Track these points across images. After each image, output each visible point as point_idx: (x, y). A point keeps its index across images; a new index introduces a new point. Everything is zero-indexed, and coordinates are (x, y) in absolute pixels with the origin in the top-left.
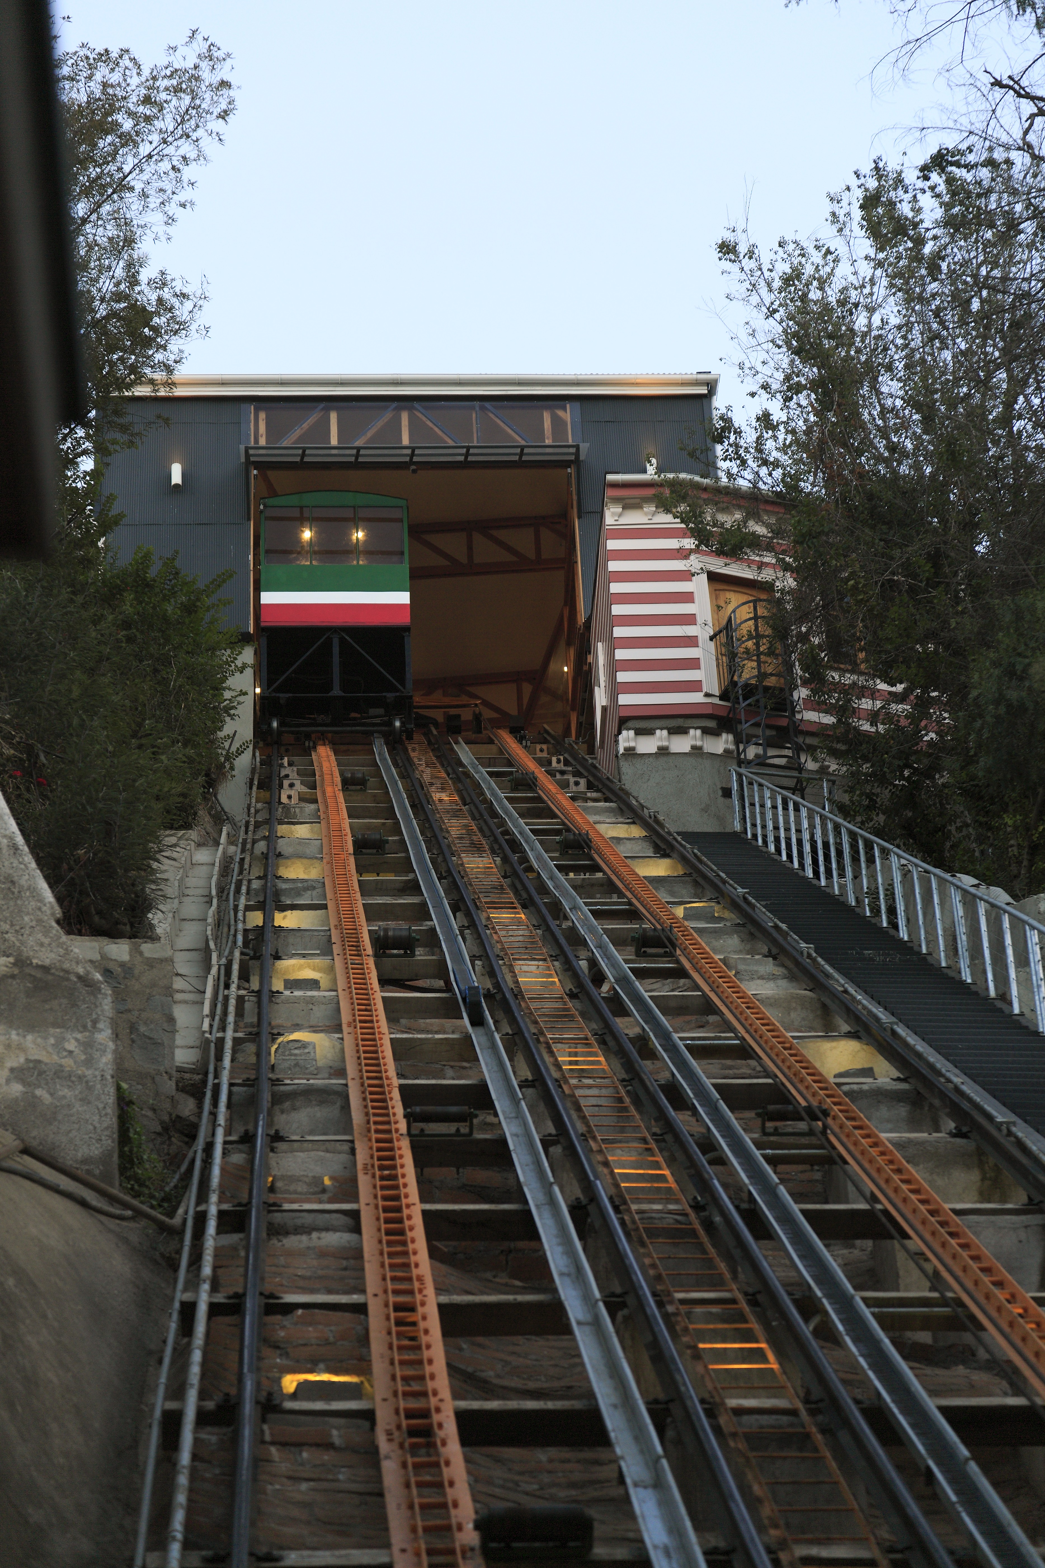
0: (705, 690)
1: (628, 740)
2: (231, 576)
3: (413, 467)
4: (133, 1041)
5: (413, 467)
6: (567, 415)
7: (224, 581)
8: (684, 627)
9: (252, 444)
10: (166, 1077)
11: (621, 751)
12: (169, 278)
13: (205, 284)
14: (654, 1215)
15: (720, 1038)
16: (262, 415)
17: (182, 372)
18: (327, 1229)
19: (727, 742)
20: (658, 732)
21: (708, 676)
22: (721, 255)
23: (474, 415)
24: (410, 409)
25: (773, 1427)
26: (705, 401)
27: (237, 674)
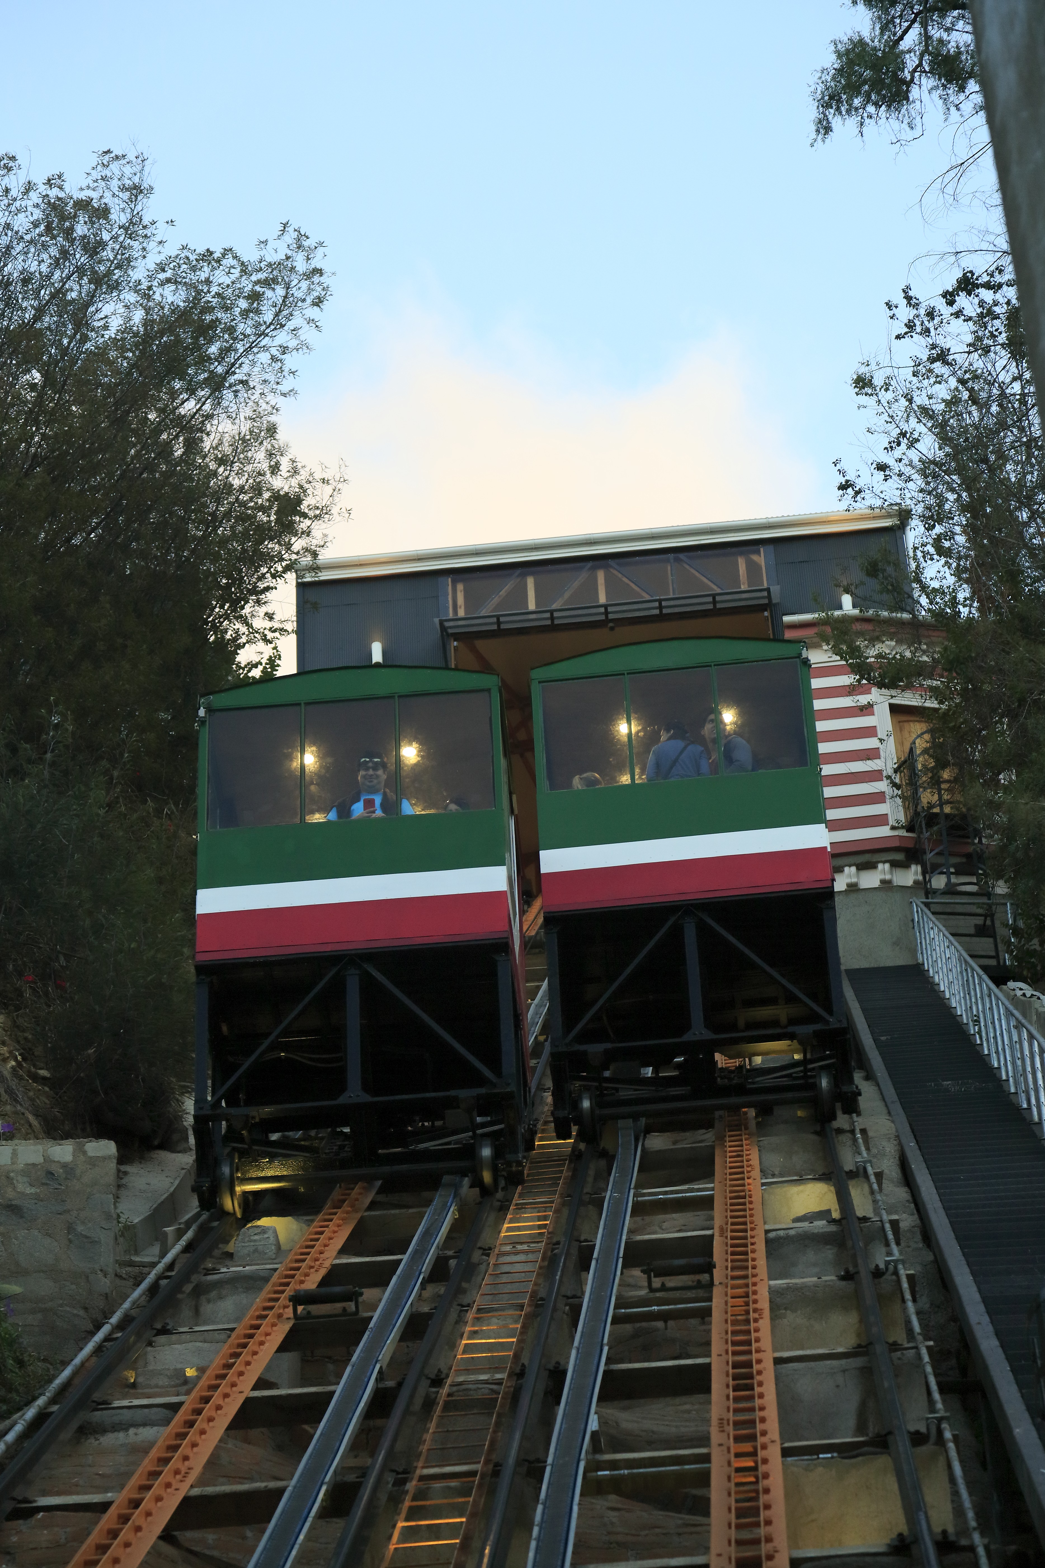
0: (891, 823)
3: (611, 625)
4: (70, 1241)
5: (611, 625)
6: (760, 559)
8: (847, 764)
9: (451, 615)
10: (100, 1275)
12: (299, 465)
13: (343, 467)
14: (470, 1386)
16: (460, 587)
17: (325, 556)
18: (144, 1425)
19: (916, 873)
20: (846, 869)
21: (893, 810)
22: (857, 390)
23: (669, 568)
24: (606, 567)
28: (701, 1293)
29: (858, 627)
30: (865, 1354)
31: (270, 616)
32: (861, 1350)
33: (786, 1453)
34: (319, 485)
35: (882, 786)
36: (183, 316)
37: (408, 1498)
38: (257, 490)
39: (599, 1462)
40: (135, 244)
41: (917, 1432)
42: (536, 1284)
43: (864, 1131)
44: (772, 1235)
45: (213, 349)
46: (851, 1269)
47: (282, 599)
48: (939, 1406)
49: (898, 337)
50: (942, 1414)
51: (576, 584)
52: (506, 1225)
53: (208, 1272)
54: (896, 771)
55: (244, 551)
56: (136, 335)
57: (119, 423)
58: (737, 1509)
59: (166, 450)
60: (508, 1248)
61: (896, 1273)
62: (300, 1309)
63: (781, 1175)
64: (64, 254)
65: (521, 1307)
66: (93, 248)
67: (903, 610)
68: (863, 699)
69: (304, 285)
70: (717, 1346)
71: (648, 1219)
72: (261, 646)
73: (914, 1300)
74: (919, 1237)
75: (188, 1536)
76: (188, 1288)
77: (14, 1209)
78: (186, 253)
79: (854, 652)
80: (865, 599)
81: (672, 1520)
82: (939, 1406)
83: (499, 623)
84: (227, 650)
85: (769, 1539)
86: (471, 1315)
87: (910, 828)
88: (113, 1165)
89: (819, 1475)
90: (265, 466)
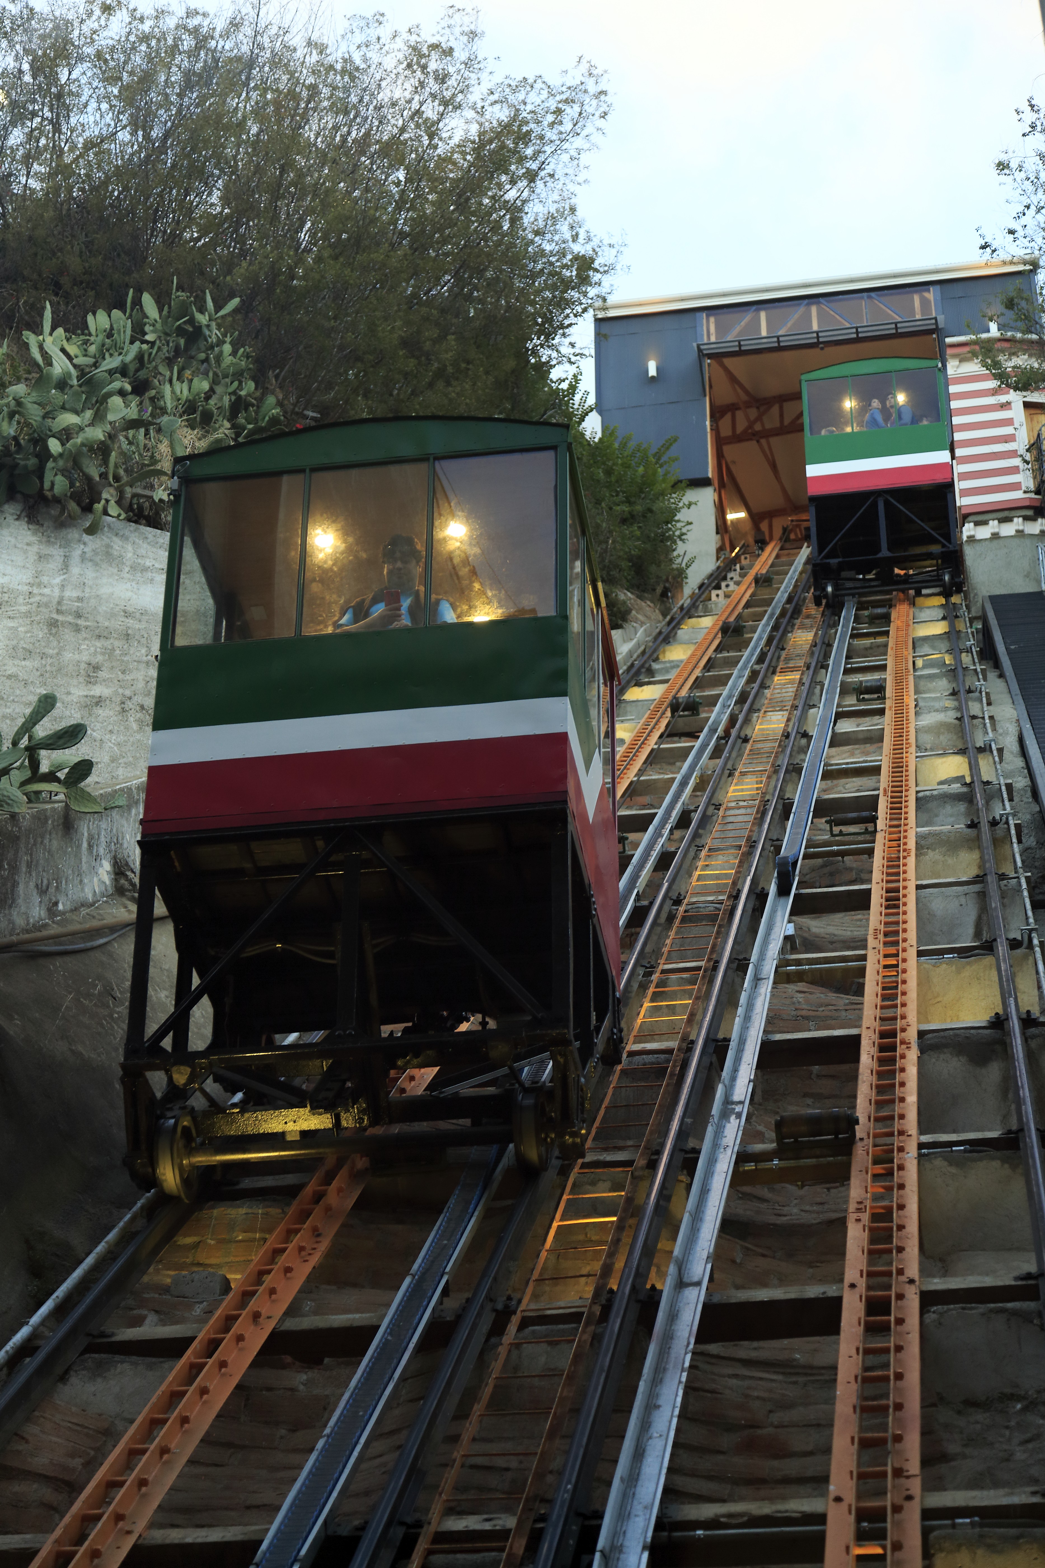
1: (969, 530)
2: (675, 440)
6: (931, 295)
7: (671, 444)
9: (705, 341)
11: (965, 538)
12: (592, 235)
15: (866, 762)
16: (712, 319)
17: (612, 300)
20: (991, 522)
21: (1026, 480)
24: (818, 303)
25: (653, 1063)
26: (1031, 275)
27: (686, 509)
28: (868, 837)
29: (999, 345)
30: (982, 882)
31: (572, 345)
32: (979, 879)
33: (920, 954)
34: (606, 249)
35: (1017, 462)
36: (506, 128)
37: (653, 985)
38: (563, 254)
39: (788, 960)
40: (472, 75)
41: (1015, 939)
42: (751, 831)
43: (991, 718)
44: (921, 795)
45: (529, 152)
46: (976, 821)
47: (582, 332)
48: (1031, 920)
49: (1024, 135)
50: (1033, 926)
51: (796, 316)
52: (732, 788)
54: (1028, 450)
55: (554, 297)
56: (473, 142)
57: (462, 206)
58: (882, 995)
59: (498, 225)
60: (733, 804)
61: (1007, 823)
63: (932, 750)
64: (422, 84)
65: (740, 847)
66: (442, 78)
67: (1032, 332)
68: (1003, 399)
69: (594, 102)
70: (877, 876)
71: (835, 782)
72: (567, 366)
73: (1020, 841)
74: (1029, 794)
78: (507, 82)
79: (996, 364)
80: (1004, 326)
81: (843, 1000)
82: (1031, 920)
83: (740, 346)
84: (544, 369)
85: (903, 1017)
86: (703, 854)
87: (1037, 492)
89: (943, 970)
90: (568, 235)
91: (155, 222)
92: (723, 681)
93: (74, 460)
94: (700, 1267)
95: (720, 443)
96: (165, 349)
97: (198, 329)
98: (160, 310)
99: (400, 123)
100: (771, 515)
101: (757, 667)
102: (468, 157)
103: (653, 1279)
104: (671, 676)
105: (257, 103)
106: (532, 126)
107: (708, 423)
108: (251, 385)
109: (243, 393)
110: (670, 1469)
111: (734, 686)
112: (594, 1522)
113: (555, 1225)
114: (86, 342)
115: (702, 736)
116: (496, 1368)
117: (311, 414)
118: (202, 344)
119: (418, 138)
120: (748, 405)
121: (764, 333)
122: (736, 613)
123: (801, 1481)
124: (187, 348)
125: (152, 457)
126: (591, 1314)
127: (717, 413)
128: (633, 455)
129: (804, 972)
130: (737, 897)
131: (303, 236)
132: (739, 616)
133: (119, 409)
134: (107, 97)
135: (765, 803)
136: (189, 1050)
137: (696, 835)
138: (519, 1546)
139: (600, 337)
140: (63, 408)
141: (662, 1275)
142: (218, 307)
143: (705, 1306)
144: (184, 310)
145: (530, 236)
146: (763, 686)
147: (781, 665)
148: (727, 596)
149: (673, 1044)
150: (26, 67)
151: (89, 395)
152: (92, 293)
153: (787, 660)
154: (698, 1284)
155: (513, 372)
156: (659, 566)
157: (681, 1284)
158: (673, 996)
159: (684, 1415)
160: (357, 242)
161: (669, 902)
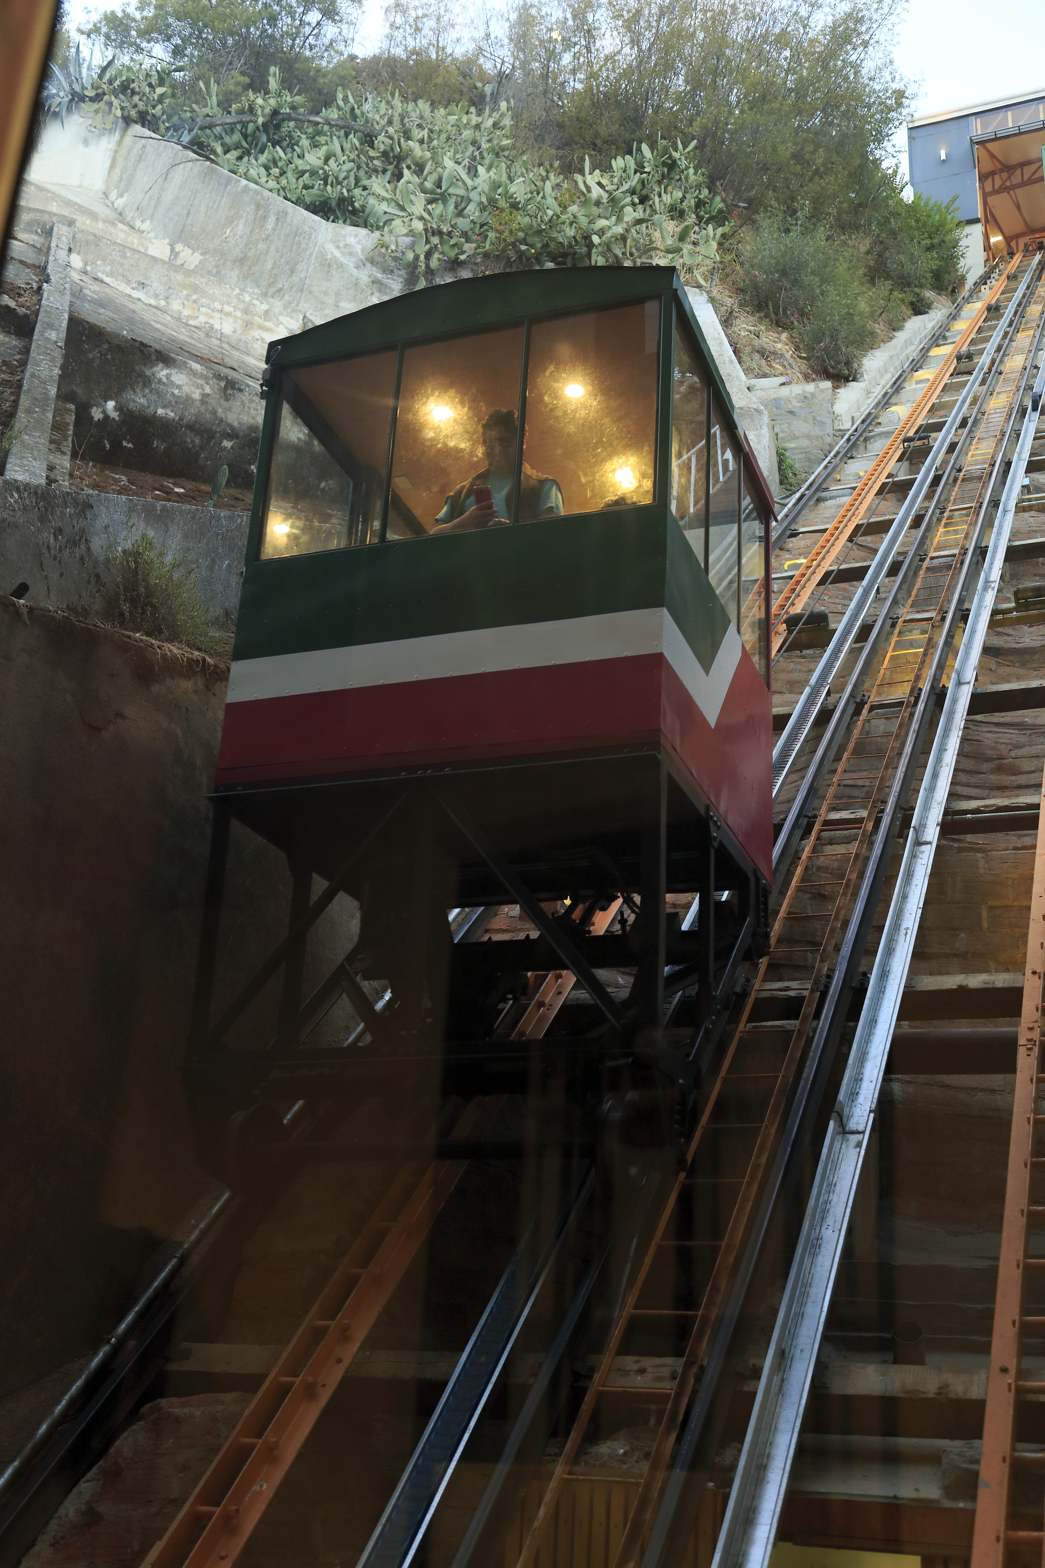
17: (917, 116)
31: (894, 146)
36: (849, 16)
45: (863, 29)
47: (899, 138)
53: (870, 431)
56: (830, 27)
57: (825, 68)
62: (906, 444)
75: (860, 540)
76: (862, 439)
77: (791, 413)
84: (877, 163)
88: (831, 391)
90: (889, 78)
91: (647, 100)
92: (987, 339)
93: (608, 246)
94: (970, 675)
95: (985, 196)
96: (656, 175)
97: (674, 162)
98: (652, 154)
99: (786, 21)
100: (1017, 237)
101: (1008, 329)
102: (828, 37)
103: (944, 681)
104: (957, 339)
105: (702, 19)
106: (865, 12)
107: (977, 184)
108: (707, 191)
109: (701, 197)
110: (952, 783)
111: (994, 342)
112: (910, 812)
113: (889, 655)
114: (612, 177)
115: (975, 373)
116: (856, 732)
117: (742, 205)
118: (677, 170)
119: (797, 29)
120: (1002, 171)
121: (1010, 125)
122: (996, 299)
123: (1027, 787)
124: (669, 174)
125: (651, 240)
126: (909, 702)
127: (983, 178)
128: (932, 209)
129: (1033, 505)
130: (994, 465)
131: (733, 98)
132: (998, 300)
133: (630, 215)
134: (616, 28)
135: (1012, 409)
136: (264, 557)
137: (971, 431)
138: (870, 826)
139: (911, 139)
140: (599, 216)
141: (949, 678)
142: (685, 146)
143: (973, 695)
144: (666, 151)
145: (867, 81)
146: (1011, 340)
147: (1022, 327)
148: (990, 289)
149: (956, 551)
150: (569, 16)
151: (613, 207)
152: (614, 147)
153: (1026, 323)
154: (969, 683)
155: (859, 166)
156: (949, 274)
157: (959, 683)
158: (957, 524)
159: (961, 754)
160: (763, 98)
161: (955, 471)
